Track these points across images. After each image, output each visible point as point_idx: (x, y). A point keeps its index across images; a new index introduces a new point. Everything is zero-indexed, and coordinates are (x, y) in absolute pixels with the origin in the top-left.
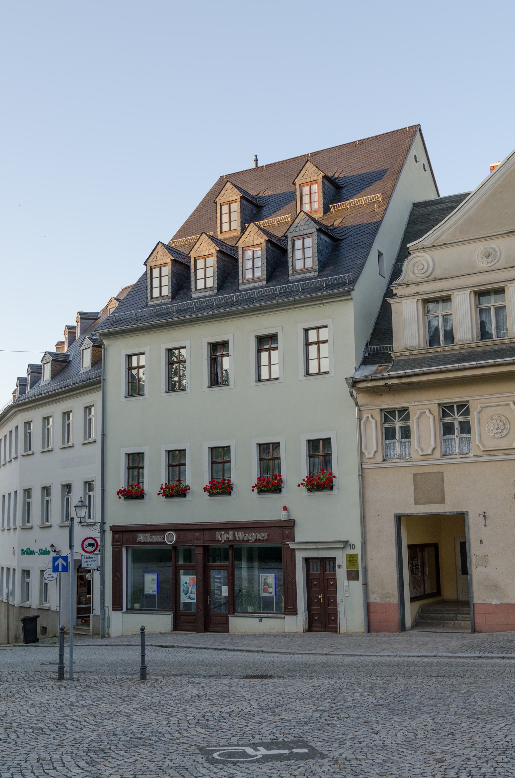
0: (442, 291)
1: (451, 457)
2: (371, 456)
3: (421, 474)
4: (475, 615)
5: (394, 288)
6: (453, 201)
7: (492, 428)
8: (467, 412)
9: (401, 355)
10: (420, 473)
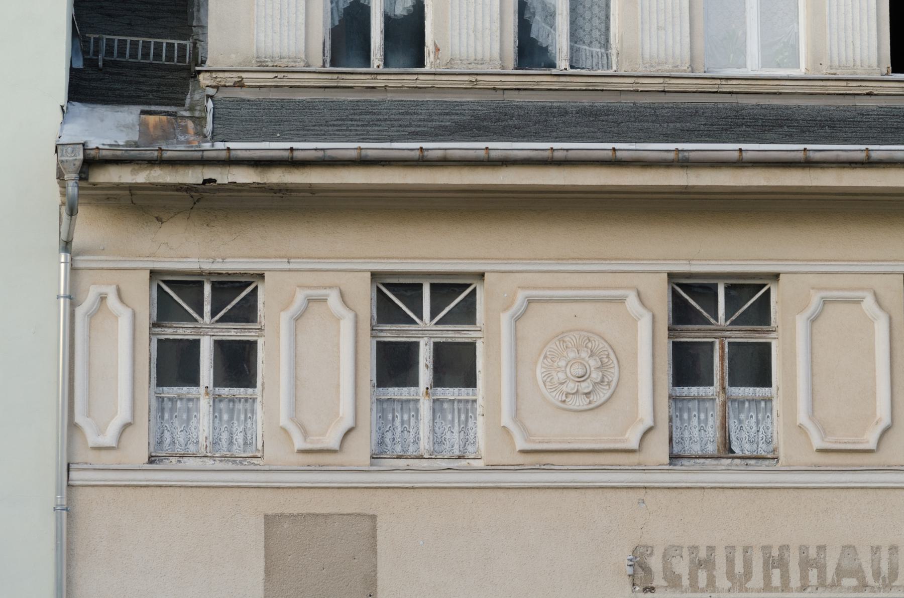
1: (402, 463)
2: (109, 439)
3: (294, 518)
7: (561, 376)
9: (240, 84)
10: (291, 515)
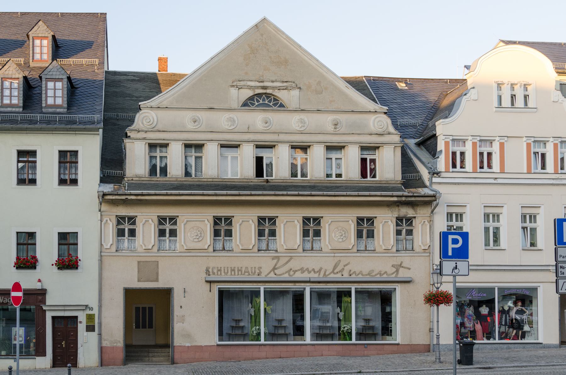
0: (164, 140)
1: (163, 251)
2: (108, 247)
4: (175, 353)
5: (129, 132)
6: (135, 75)
8: (134, 223)
9: (132, 180)
